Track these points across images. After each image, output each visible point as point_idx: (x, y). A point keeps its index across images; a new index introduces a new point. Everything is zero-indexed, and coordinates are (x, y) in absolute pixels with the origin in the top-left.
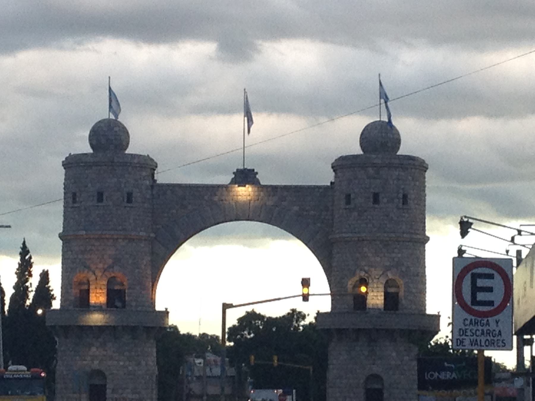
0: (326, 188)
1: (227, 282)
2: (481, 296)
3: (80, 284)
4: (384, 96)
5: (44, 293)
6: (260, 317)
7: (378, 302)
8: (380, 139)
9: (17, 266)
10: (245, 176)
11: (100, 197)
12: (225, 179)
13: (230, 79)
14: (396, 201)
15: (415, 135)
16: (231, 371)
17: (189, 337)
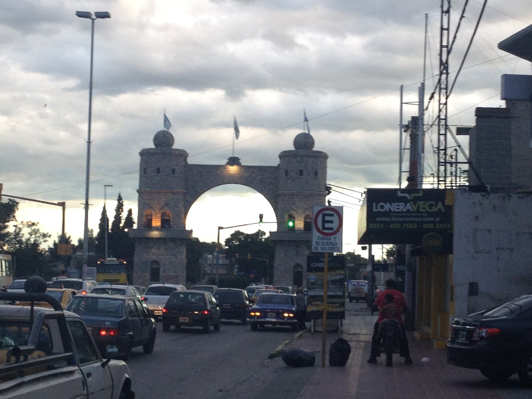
0: (276, 167)
1: (223, 216)
2: (327, 225)
3: (148, 215)
4: (306, 120)
5: (129, 221)
6: (242, 234)
7: (300, 226)
8: (304, 142)
9: (116, 206)
10: (234, 161)
11: (158, 171)
12: (224, 162)
13: (232, 109)
14: (311, 174)
15: (322, 139)
16: (227, 262)
17: (204, 244)
